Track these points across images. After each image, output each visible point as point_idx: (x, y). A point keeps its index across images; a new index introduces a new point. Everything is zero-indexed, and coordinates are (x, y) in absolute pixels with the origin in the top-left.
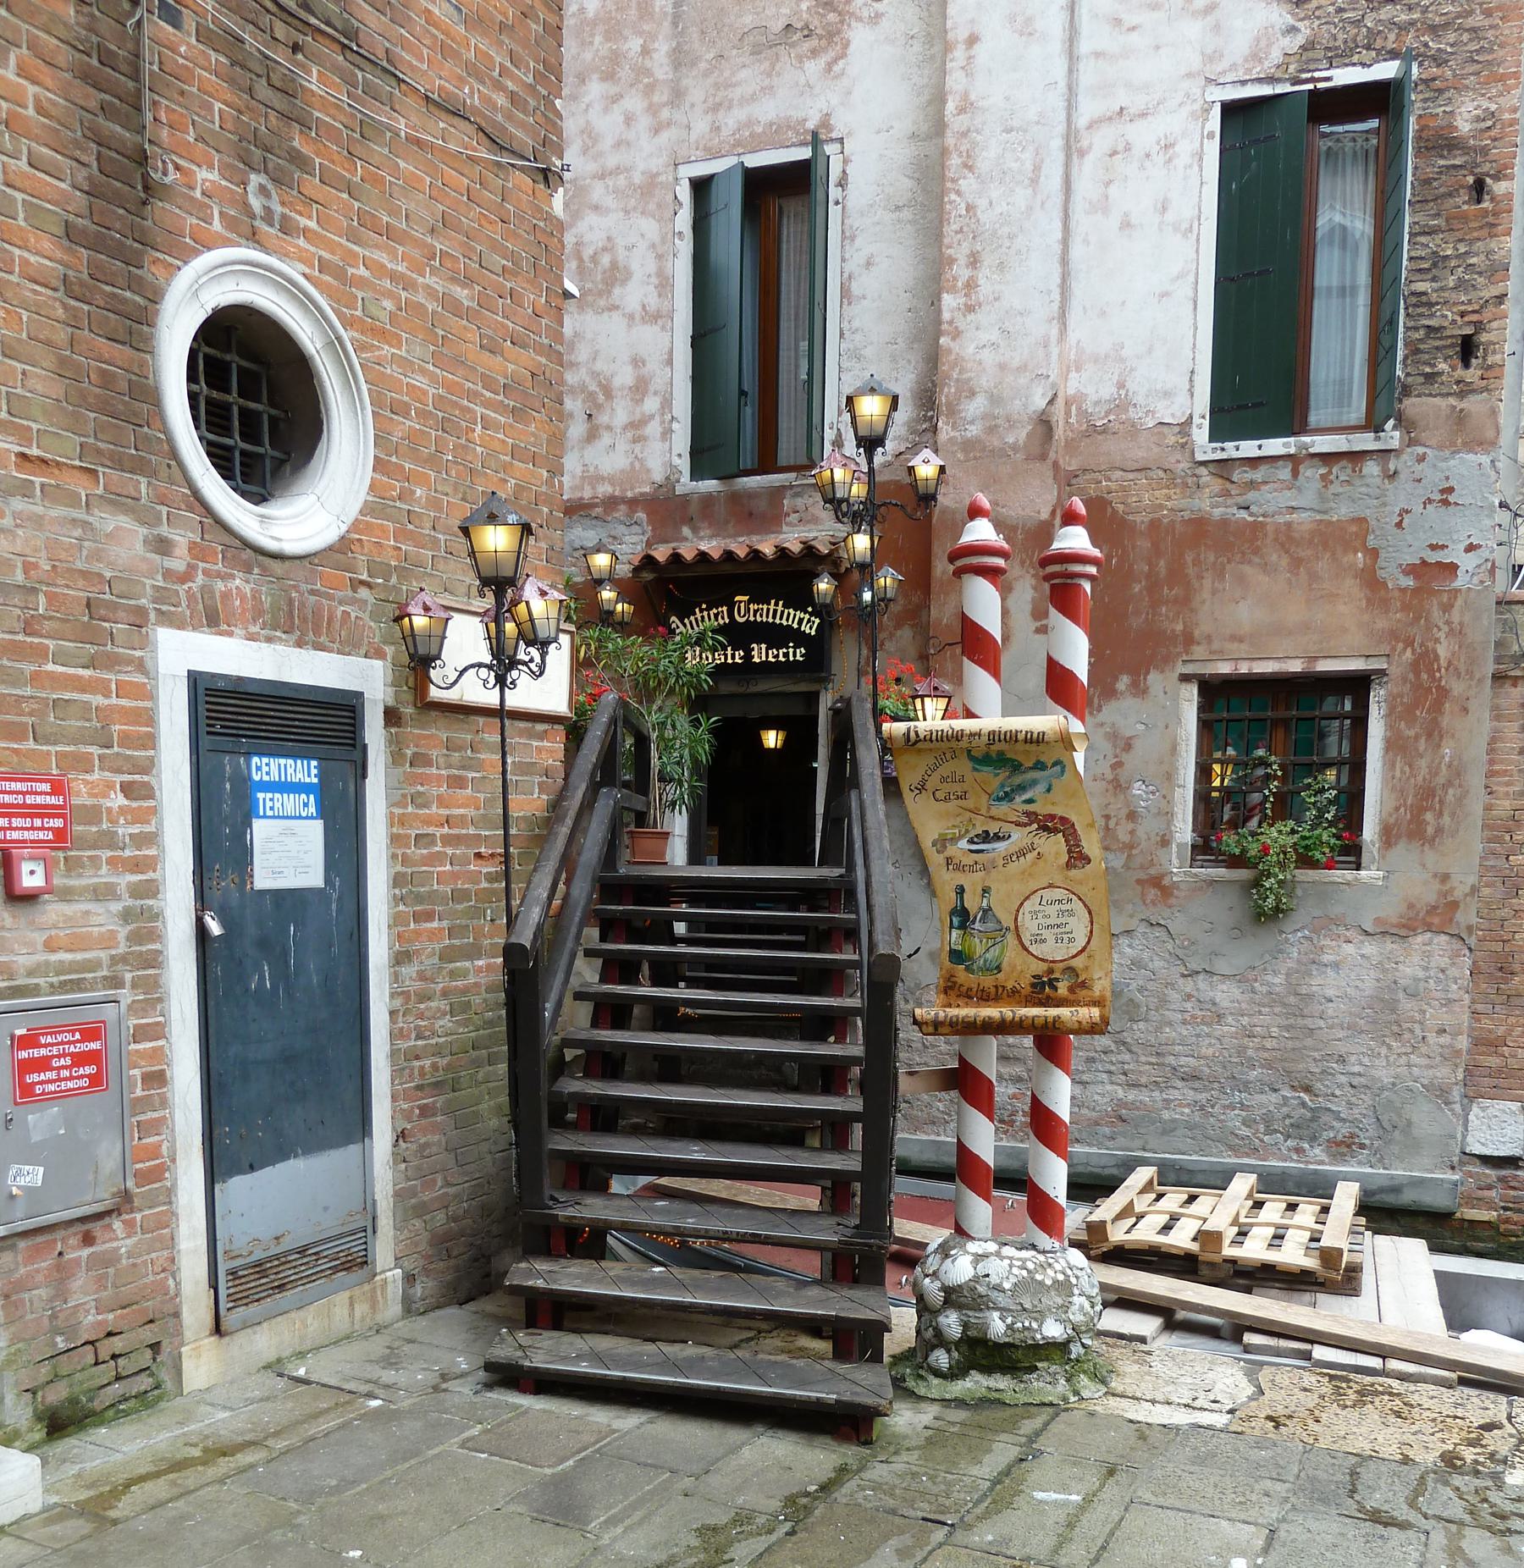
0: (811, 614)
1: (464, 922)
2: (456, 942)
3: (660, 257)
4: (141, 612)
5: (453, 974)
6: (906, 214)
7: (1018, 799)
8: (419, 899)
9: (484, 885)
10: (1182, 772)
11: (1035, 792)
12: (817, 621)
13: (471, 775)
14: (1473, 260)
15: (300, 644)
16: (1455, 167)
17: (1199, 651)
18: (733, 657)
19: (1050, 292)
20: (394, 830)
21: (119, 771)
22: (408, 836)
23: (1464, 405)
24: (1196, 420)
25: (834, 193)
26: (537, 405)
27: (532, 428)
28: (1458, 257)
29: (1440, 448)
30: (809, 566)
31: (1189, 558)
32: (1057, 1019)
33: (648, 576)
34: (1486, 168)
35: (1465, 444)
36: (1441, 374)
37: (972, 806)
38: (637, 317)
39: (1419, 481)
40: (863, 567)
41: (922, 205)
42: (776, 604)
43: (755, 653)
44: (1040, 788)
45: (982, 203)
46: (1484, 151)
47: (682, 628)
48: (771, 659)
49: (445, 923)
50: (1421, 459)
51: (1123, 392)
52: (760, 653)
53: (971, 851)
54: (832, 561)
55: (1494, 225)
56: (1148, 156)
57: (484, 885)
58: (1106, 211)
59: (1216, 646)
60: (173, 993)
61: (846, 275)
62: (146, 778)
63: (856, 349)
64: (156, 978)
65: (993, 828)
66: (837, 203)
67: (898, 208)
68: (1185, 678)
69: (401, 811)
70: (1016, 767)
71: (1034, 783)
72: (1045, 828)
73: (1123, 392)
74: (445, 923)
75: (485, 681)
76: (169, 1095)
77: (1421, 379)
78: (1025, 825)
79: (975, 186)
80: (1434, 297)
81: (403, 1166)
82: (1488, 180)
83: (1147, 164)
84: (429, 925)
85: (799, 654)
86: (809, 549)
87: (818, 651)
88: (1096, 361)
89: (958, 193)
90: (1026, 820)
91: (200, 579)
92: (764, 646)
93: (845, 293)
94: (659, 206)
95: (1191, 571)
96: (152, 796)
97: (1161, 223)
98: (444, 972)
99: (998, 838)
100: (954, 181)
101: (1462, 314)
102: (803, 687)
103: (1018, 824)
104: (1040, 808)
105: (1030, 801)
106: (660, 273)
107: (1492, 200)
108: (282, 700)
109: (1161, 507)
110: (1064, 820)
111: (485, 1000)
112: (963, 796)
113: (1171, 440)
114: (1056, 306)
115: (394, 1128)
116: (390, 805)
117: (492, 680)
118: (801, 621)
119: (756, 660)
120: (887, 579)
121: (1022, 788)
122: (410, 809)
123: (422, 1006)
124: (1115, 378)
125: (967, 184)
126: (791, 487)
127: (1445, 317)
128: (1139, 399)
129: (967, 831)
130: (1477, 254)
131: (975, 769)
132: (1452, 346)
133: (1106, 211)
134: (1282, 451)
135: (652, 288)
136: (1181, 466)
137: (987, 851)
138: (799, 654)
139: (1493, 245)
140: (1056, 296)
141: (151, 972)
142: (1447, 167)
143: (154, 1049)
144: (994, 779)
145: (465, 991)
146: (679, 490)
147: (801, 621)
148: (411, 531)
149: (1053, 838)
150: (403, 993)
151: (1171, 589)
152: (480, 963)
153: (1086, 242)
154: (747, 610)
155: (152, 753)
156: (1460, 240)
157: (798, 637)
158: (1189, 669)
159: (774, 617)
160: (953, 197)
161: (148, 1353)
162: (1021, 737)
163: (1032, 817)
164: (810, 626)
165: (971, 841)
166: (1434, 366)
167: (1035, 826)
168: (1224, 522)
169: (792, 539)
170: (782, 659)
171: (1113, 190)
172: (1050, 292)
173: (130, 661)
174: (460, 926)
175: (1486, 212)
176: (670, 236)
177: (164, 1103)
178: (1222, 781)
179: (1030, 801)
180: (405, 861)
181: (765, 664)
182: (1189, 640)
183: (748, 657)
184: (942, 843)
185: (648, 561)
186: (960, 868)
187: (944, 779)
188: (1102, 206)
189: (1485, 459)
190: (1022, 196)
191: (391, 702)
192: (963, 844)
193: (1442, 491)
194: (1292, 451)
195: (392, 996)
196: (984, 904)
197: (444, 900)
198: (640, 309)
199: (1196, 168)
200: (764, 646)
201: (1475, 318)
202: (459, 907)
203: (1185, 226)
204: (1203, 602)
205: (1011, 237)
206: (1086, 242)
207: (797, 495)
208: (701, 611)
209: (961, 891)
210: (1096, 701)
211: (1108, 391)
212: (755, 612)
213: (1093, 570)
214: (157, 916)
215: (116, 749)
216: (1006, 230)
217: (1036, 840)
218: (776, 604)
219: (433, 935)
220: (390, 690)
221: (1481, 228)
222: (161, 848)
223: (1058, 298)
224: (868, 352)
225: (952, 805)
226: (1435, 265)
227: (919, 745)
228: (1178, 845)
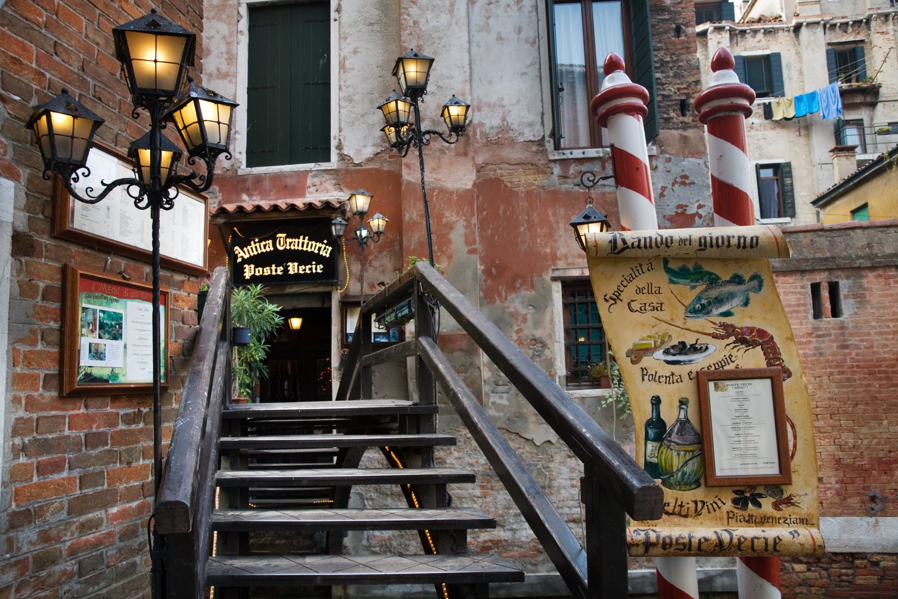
0: (326, 244)
1: (98, 468)
2: (89, 491)
3: (228, 44)
5: (85, 528)
6: (376, 27)
7: (715, 312)
8: (44, 446)
9: (122, 427)
10: (557, 333)
11: (733, 305)
12: (330, 248)
14: (681, 64)
16: (665, 19)
17: (561, 264)
18: (276, 271)
19: (463, 67)
20: (18, 369)
22: (35, 378)
23: (686, 133)
24: (547, 138)
25: (333, 15)
26: (183, 9)
28: (673, 62)
29: (678, 155)
30: (327, 214)
31: (550, 212)
32: (777, 540)
33: (220, 221)
34: (681, 21)
35: (689, 153)
36: (673, 118)
37: (668, 319)
38: (214, 75)
39: (669, 171)
40: (362, 214)
41: (385, 23)
42: (304, 239)
44: (736, 302)
45: (422, 21)
46: (679, 13)
47: (242, 254)
49: (76, 473)
50: (669, 160)
51: (505, 123)
52: (293, 268)
53: (668, 362)
54: (341, 209)
55: (688, 48)
56: (508, 5)
57: (122, 427)
58: (488, 31)
59: (570, 260)
61: (342, 57)
63: (349, 96)
65: (690, 340)
66: (335, 20)
67: (371, 24)
68: (554, 279)
69: (28, 348)
70: (713, 281)
71: (731, 296)
73: (505, 123)
74: (76, 473)
75: (138, 200)
77: (662, 121)
78: (722, 337)
79: (418, 12)
80: (664, 81)
82: (683, 27)
83: (508, 9)
84: (56, 476)
86: (327, 205)
87: (331, 265)
88: (489, 106)
89: (409, 15)
90: (722, 332)
92: (296, 264)
93: (342, 66)
94: (228, 17)
95: (552, 219)
97: (518, 39)
98: (73, 528)
99: (695, 349)
100: (405, 8)
101: (679, 89)
102: (321, 289)
103: (715, 336)
105: (727, 314)
106: (229, 52)
107: (686, 36)
109: (532, 184)
110: (762, 333)
111: (120, 550)
112: (659, 307)
113: (534, 148)
114: (467, 74)
118: (320, 249)
119: (291, 272)
120: (377, 222)
121: (719, 301)
122: (39, 347)
123: (44, 573)
124: (500, 116)
125: (414, 10)
126: (311, 171)
127: (671, 90)
128: (515, 127)
129: (663, 343)
130: (682, 61)
131: (671, 282)
132: (676, 104)
133: (488, 31)
134: (596, 155)
135: (223, 60)
136: (541, 162)
137: (685, 362)
138: (319, 269)
139: (690, 57)
140: (467, 69)
142: (662, 20)
144: (689, 293)
145: (98, 543)
146: (240, 173)
147: (320, 249)
148: (58, 63)
149: (752, 351)
150: (18, 563)
151: (541, 229)
152: (114, 510)
153: (479, 46)
154: (284, 243)
156: (673, 54)
157: (319, 259)
158: (557, 274)
159: (303, 246)
160: (406, 17)
162: (734, 241)
163: (729, 330)
164: (326, 251)
165: (666, 352)
166: (668, 114)
167: (733, 339)
168: (568, 192)
169: (315, 197)
170: (308, 271)
171: (491, 21)
172: (463, 67)
174: (93, 474)
175: (683, 42)
176: (235, 32)
179: (727, 314)
180: (31, 404)
181: (297, 275)
182: (555, 258)
183: (286, 270)
184: (637, 354)
185: (222, 211)
186: (655, 378)
187: (640, 291)
188: (486, 28)
189: (701, 161)
190: (444, 18)
191: (22, 226)
192: (659, 354)
193: (682, 177)
194: (601, 155)
196: (682, 416)
197: (76, 445)
198: (216, 71)
199: (534, 13)
200: (296, 264)
201: (686, 91)
202: (93, 452)
203: (531, 40)
204: (560, 236)
205: (440, 38)
206: (479, 46)
207: (316, 176)
208: (255, 243)
209: (656, 402)
210: (504, 293)
211: (496, 122)
212: (290, 244)
216: (436, 35)
217: (734, 352)
218: (304, 239)
219: (61, 488)
220: (23, 216)
221: (682, 49)
223: (468, 70)
224: (356, 98)
225: (649, 316)
226: (662, 65)
227: (626, 253)
228: (559, 377)
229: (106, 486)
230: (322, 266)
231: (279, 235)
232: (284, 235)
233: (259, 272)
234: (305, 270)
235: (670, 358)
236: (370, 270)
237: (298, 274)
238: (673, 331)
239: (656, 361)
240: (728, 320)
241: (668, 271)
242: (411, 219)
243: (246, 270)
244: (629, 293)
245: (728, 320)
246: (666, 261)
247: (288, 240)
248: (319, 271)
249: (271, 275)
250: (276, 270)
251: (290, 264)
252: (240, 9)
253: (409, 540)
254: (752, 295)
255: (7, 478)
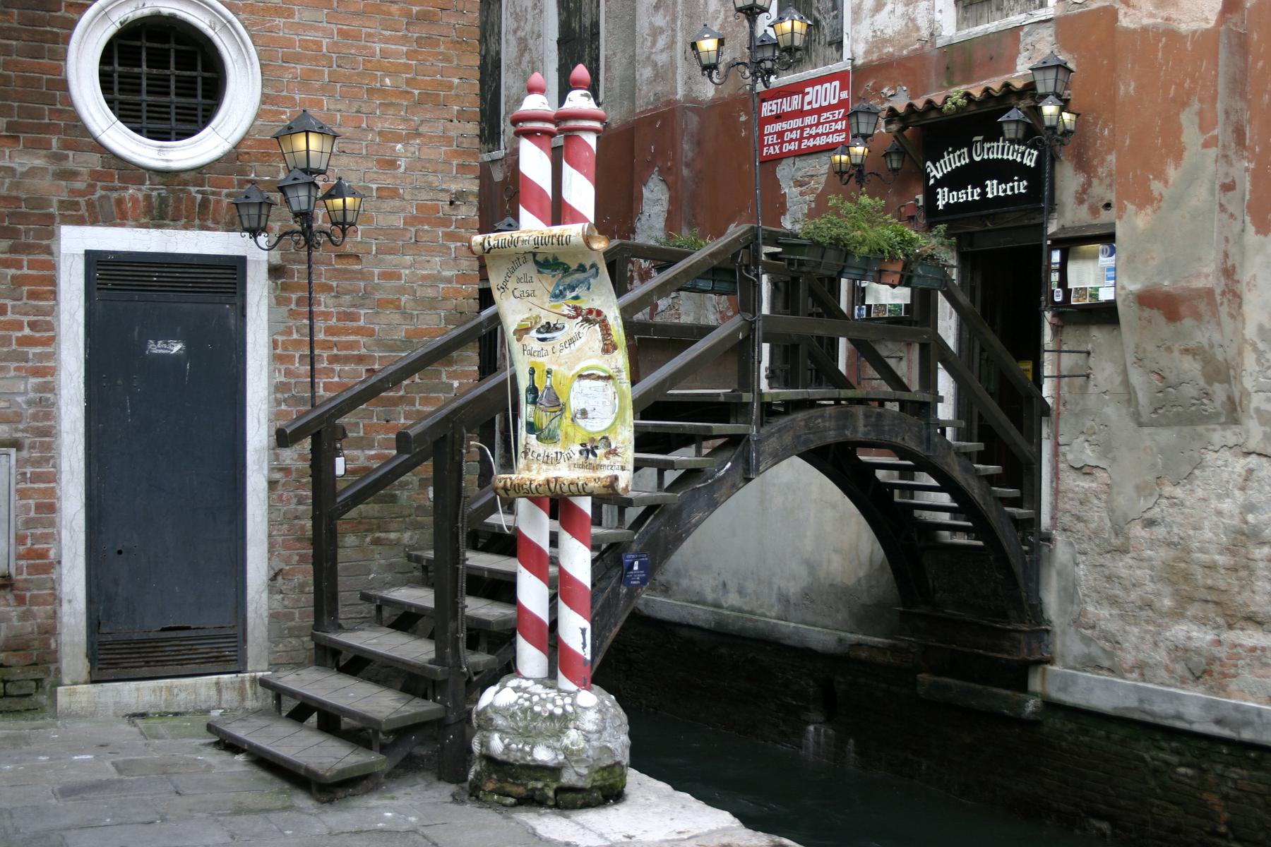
4: (51, 217)
12: (1036, 153)
13: (362, 312)
15: (186, 228)
21: (26, 314)
27: (442, 49)
43: (988, 189)
47: (935, 172)
48: (1001, 194)
52: (994, 189)
60: (64, 452)
62: (48, 318)
64: (50, 444)
69: (285, 338)
72: (586, 320)
76: (57, 520)
81: (280, 597)
85: (1021, 187)
87: (1040, 182)
91: (99, 193)
92: (995, 182)
96: (52, 329)
103: (569, 318)
104: (585, 306)
105: (576, 298)
108: (130, 264)
115: (270, 567)
116: (272, 332)
117: (303, 243)
119: (990, 196)
138: (1021, 187)
141: (47, 439)
143: (46, 489)
155: (52, 303)
161: (33, 684)
170: (1009, 193)
173: (40, 246)
177: (52, 524)
178: (919, 276)
183: (983, 193)
184: (522, 332)
187: (519, 280)
195: (271, 470)
200: (995, 182)
213: (597, 125)
214: (53, 404)
215: (25, 300)
222: (58, 360)
229: (361, 434)
230: (1025, 183)
231: (976, 138)
232: (980, 138)
233: (962, 196)
234: (1005, 191)
235: (541, 336)
236: (1095, 182)
237: (998, 197)
238: (543, 313)
239: (532, 339)
240: (577, 303)
241: (537, 263)
242: (1127, 93)
243: (939, 197)
244: (510, 286)
245: (577, 303)
246: (534, 255)
247: (987, 145)
248: (1023, 191)
249: (967, 201)
250: (971, 194)
251: (988, 182)
252: (20, 169)
253: (1130, 624)
254: (592, 280)
255: (272, 417)
